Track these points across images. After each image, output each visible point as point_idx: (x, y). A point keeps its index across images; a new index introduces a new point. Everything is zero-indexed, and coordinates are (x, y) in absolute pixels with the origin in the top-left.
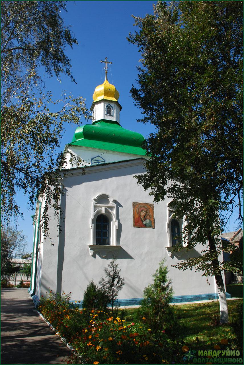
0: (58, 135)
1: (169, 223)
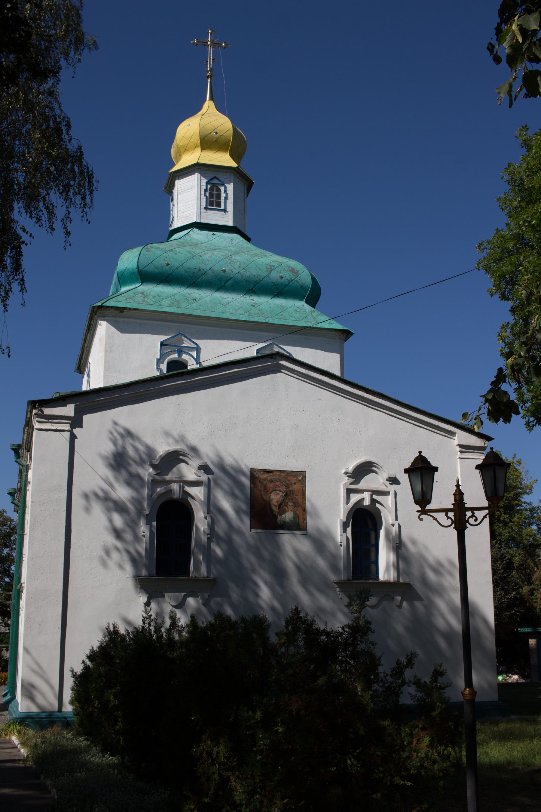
1: (345, 520)
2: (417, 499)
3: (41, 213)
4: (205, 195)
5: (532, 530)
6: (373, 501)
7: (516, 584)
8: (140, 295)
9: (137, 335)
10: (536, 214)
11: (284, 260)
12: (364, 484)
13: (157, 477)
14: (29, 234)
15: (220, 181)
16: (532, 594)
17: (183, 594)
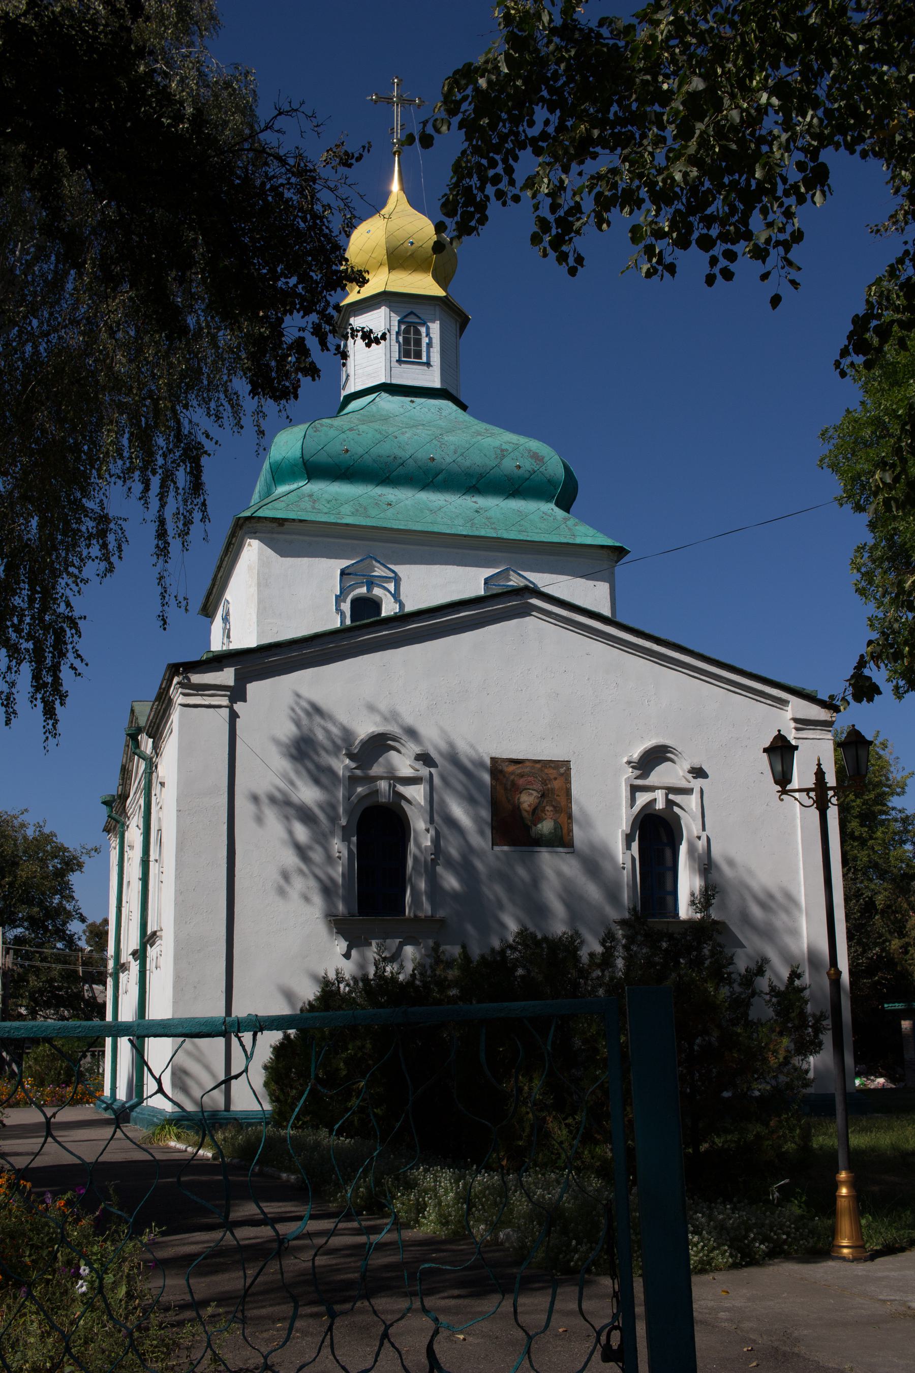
0: (87, 542)
1: (628, 831)
2: (777, 778)
3: (221, 408)
4: (398, 341)
5: (905, 852)
6: (670, 803)
7: (880, 936)
8: (307, 499)
9: (306, 560)
10: (903, 402)
11: (522, 440)
12: (654, 779)
13: (358, 772)
14: (214, 441)
15: (419, 318)
16: (906, 952)
17: (398, 941)
